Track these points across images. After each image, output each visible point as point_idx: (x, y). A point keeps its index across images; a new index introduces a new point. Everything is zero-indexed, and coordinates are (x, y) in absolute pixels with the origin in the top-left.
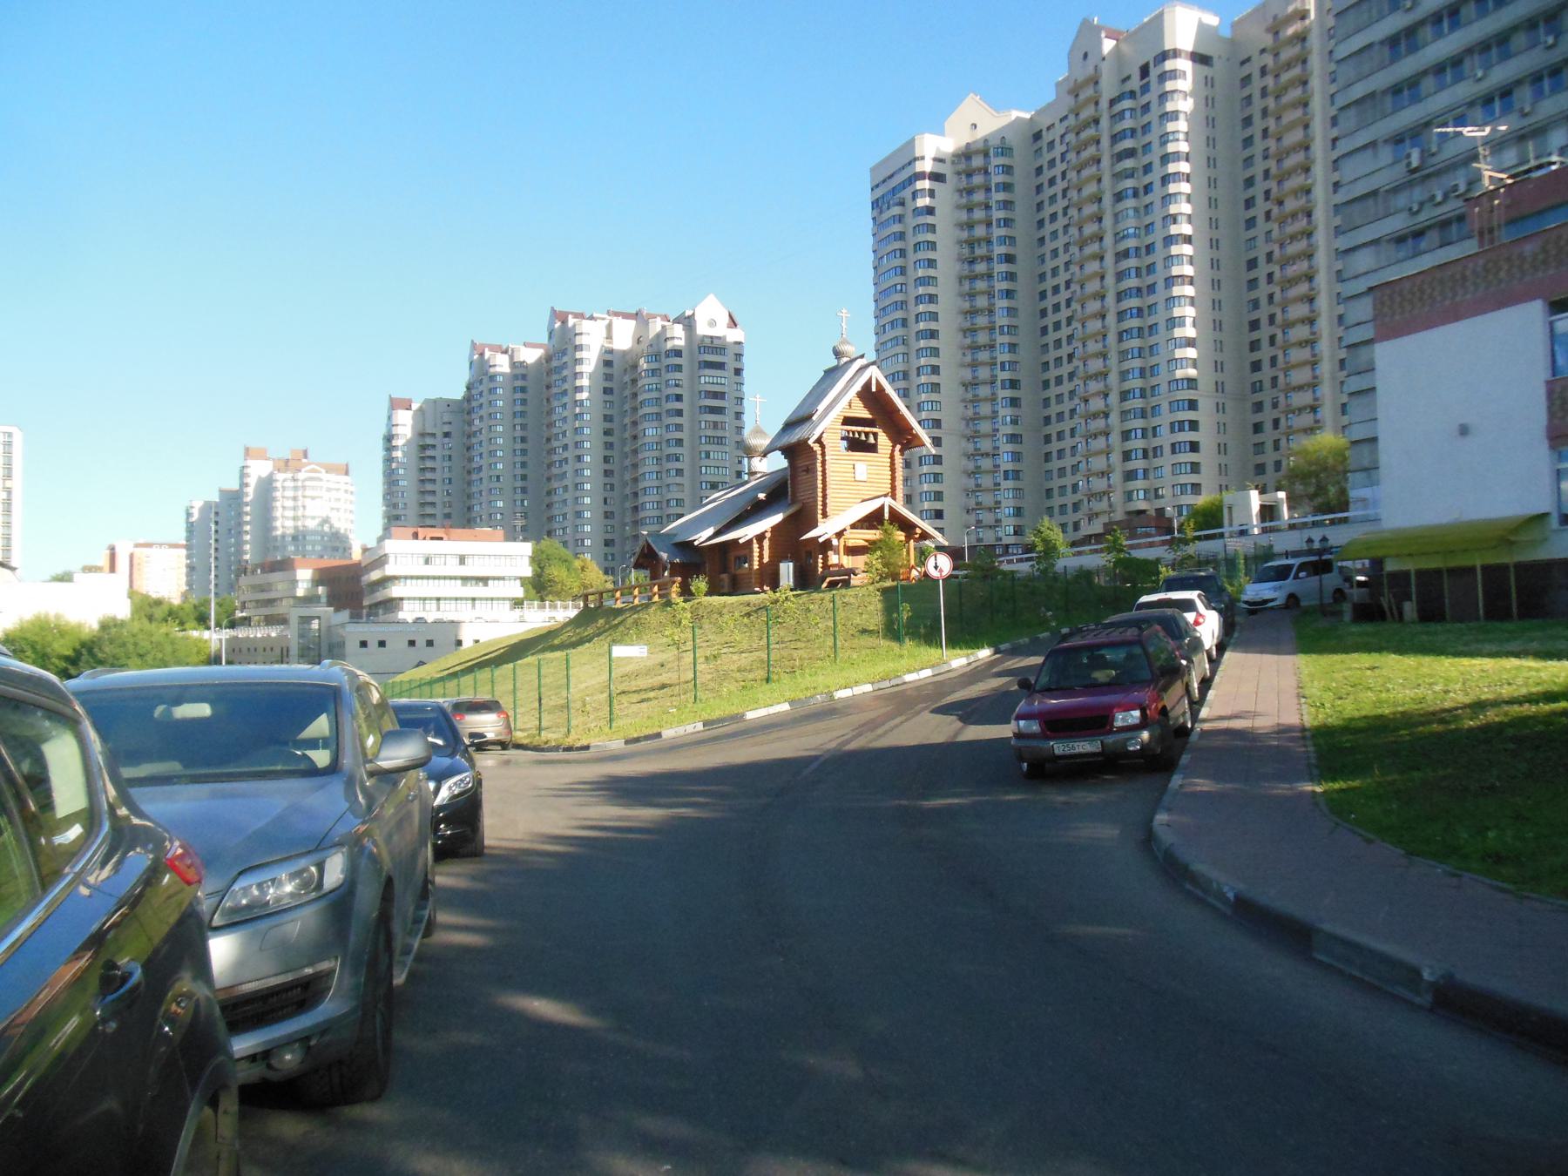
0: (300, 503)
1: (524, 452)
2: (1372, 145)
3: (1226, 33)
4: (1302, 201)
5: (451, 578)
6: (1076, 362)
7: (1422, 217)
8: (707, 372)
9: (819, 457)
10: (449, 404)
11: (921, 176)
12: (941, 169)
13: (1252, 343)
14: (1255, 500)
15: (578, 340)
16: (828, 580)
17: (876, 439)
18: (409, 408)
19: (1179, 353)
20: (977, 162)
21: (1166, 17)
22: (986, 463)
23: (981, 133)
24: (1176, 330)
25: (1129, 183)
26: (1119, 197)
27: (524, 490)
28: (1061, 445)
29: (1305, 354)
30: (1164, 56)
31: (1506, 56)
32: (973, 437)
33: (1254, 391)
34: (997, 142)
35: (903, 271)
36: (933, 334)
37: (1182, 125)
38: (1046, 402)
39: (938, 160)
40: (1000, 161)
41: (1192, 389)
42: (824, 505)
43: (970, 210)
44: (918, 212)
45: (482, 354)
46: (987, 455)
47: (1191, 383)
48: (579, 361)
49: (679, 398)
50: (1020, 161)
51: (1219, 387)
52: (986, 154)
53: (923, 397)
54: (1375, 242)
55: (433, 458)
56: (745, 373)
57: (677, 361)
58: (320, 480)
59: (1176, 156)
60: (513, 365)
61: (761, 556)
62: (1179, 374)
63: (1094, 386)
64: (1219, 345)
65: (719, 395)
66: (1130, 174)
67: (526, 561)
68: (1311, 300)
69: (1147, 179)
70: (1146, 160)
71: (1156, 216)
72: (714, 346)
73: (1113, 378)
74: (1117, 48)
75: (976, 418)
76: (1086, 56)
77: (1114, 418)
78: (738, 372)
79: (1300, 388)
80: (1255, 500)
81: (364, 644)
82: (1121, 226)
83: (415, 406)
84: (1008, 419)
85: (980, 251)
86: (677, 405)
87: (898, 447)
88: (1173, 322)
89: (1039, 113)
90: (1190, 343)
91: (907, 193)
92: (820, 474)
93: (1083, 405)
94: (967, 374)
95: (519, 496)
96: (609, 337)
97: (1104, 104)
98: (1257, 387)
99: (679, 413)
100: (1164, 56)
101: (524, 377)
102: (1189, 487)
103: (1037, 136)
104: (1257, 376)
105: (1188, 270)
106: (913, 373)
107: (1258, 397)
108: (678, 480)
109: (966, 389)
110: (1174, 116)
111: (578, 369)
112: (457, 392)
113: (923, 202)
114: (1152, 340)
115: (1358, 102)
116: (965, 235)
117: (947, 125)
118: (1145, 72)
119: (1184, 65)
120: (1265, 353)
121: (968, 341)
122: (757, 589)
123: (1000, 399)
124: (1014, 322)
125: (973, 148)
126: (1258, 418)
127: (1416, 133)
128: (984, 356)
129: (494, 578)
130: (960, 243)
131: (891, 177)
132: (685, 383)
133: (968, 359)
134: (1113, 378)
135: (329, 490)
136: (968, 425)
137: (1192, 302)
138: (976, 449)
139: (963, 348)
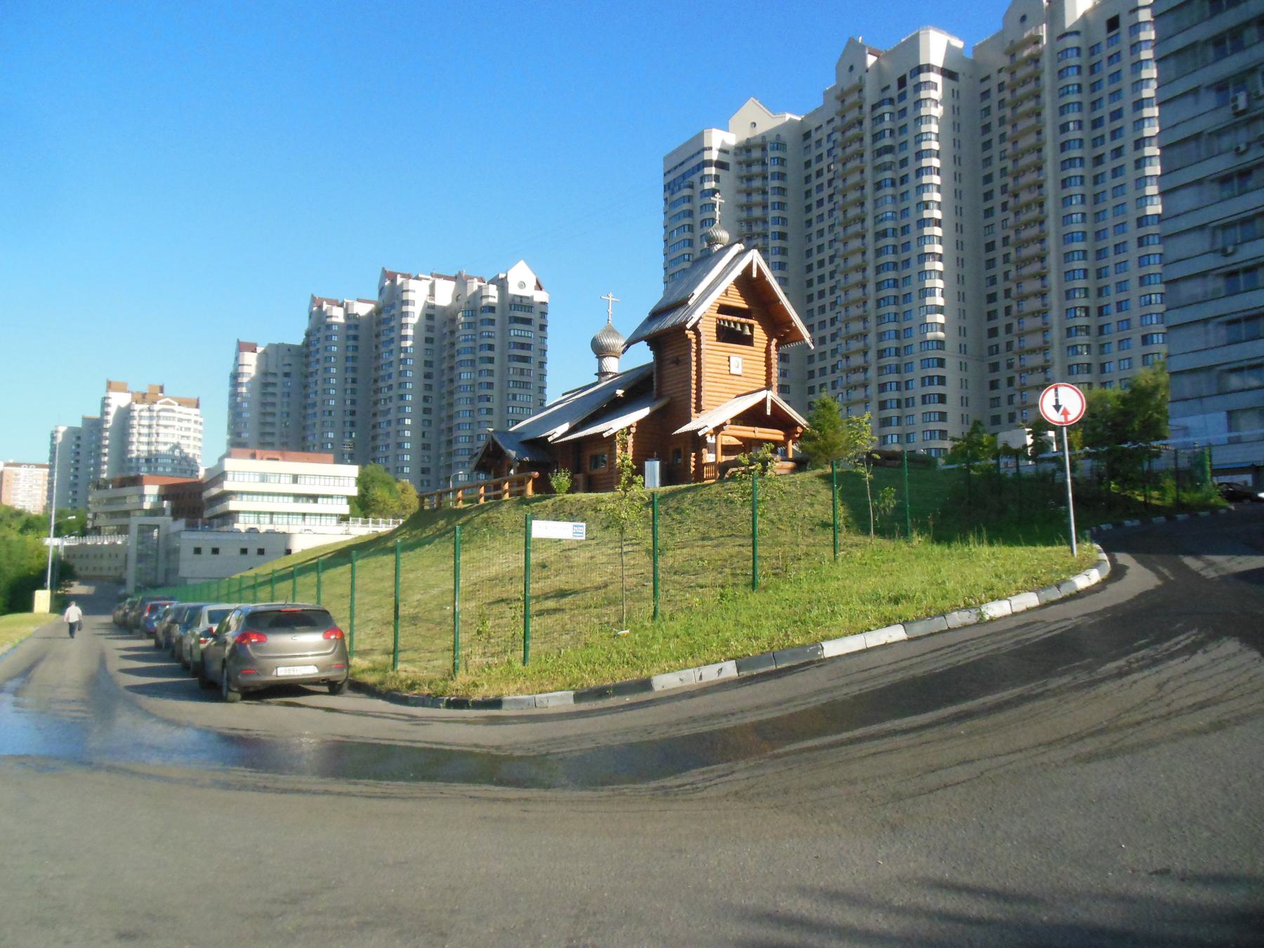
0: (154, 431)
2: (1195, 92)
3: (969, 55)
6: (838, 325)
9: (694, 345)
10: (290, 348)
11: (708, 163)
12: (725, 159)
15: (405, 297)
18: (254, 351)
20: (756, 154)
23: (759, 130)
25: (888, 174)
26: (879, 186)
27: (353, 424)
29: (1038, 322)
30: (920, 69)
33: (991, 354)
35: (691, 228)
42: (699, 398)
45: (320, 307)
47: (940, 343)
48: (406, 314)
49: (491, 347)
51: (963, 349)
52: (764, 149)
54: (1198, 182)
56: (548, 329)
57: (491, 316)
58: (173, 411)
59: (930, 153)
62: (930, 335)
63: (855, 345)
67: (353, 482)
70: (902, 156)
71: (911, 203)
72: (523, 304)
73: (872, 338)
74: (877, 63)
76: (851, 68)
77: (872, 373)
78: (543, 327)
79: (1033, 351)
82: (880, 211)
83: (260, 350)
86: (489, 354)
87: (774, 341)
89: (808, 116)
91: (695, 178)
92: (694, 364)
93: (844, 361)
95: (348, 429)
96: (432, 294)
97: (867, 108)
98: (994, 350)
99: (491, 360)
100: (920, 69)
101: (356, 327)
103: (807, 135)
107: (994, 359)
111: (404, 320)
116: (744, 215)
118: (902, 82)
119: (936, 78)
120: (1001, 322)
125: (753, 142)
130: (740, 221)
131: (682, 163)
132: (498, 335)
134: (872, 338)
135: (180, 420)
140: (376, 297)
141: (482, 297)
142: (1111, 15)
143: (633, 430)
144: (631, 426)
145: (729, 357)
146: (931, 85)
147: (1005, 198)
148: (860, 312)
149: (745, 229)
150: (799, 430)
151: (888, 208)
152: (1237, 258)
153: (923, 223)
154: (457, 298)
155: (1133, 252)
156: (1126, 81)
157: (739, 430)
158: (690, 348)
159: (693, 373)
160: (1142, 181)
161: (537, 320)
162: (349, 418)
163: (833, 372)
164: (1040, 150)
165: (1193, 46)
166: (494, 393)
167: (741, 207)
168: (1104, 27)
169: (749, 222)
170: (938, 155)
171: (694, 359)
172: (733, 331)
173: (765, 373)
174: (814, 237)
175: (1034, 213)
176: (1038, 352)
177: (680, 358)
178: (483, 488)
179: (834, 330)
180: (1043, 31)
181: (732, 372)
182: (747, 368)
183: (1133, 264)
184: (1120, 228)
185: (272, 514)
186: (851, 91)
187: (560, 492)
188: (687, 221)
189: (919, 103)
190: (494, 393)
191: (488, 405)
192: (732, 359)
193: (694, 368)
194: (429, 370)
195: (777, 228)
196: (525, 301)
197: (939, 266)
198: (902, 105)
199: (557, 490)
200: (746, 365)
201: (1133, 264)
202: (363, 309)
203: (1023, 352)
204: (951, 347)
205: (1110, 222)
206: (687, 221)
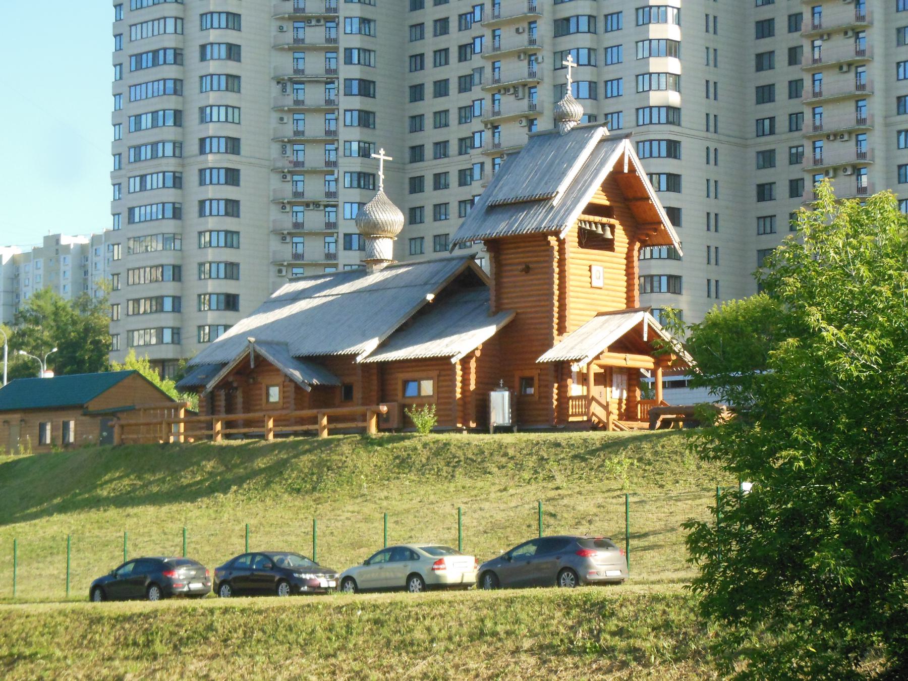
6: (476, 61)
9: (556, 254)
13: (759, 57)
16: (662, 417)
17: (613, 233)
19: (657, 64)
22: (314, 220)
24: (652, 27)
29: (847, 83)
32: (292, 173)
33: (760, 133)
38: (416, 122)
41: (672, 123)
42: (562, 318)
46: (317, 205)
47: (673, 114)
51: (712, 123)
53: (213, 98)
61: (465, 381)
62: (656, 98)
63: (510, 105)
64: (712, 57)
75: (298, 139)
79: (837, 136)
84: (355, 146)
87: (638, 245)
90: (672, 48)
92: (556, 276)
93: (487, 134)
94: (285, 64)
98: (765, 127)
102: (664, 280)
104: (766, 110)
106: (193, 54)
107: (766, 143)
109: (284, 90)
122: (459, 425)
123: (341, 112)
126: (765, 176)
128: (315, 35)
133: (288, 38)
136: (284, 151)
138: (296, 194)
143: (478, 353)
144: (477, 349)
145: (590, 267)
148: (522, 41)
150: (674, 357)
157: (614, 358)
158: (551, 257)
159: (556, 287)
171: (557, 270)
172: (591, 232)
173: (625, 284)
176: (846, 137)
177: (531, 266)
178: (326, 418)
179: (465, 69)
181: (594, 284)
182: (544, 251)
187: (424, 432)
192: (593, 268)
193: (556, 282)
199: (421, 430)
200: (607, 275)
203: (820, 134)
204: (692, 120)
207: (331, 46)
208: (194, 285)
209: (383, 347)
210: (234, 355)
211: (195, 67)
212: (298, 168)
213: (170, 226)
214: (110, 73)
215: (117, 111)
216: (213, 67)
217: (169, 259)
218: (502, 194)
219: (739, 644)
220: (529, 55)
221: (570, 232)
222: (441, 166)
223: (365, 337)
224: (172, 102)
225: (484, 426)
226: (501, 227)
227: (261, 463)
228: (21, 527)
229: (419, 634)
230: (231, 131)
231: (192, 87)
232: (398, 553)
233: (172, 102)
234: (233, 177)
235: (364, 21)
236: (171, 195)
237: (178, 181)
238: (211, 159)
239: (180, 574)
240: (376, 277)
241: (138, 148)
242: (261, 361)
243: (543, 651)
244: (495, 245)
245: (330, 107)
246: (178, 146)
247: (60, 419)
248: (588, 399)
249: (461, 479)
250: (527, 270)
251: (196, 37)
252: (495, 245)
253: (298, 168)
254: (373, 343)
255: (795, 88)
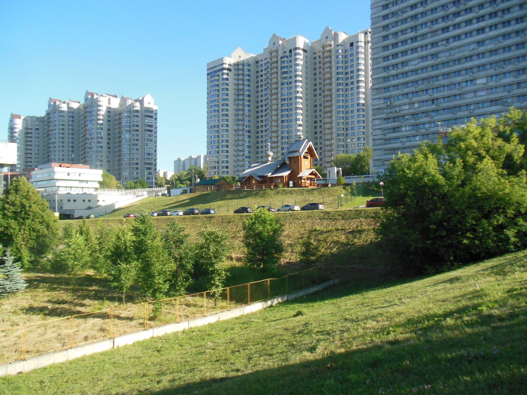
1: (73, 138)
2: (379, 98)
3: (310, 45)
4: (329, 93)
5: (76, 180)
7: (390, 115)
8: (148, 118)
11: (224, 69)
12: (230, 67)
14: (336, 169)
15: (99, 103)
18: (20, 118)
19: (298, 128)
20: (241, 67)
21: (297, 38)
22: (241, 153)
23: (242, 59)
25: (286, 81)
26: (282, 84)
27: (73, 151)
28: (262, 150)
30: (296, 49)
31: (407, 87)
34: (247, 62)
36: (227, 115)
37: (300, 68)
38: (258, 137)
39: (230, 65)
40: (248, 68)
43: (238, 80)
44: (223, 79)
45: (55, 103)
48: (100, 110)
49: (137, 126)
50: (252, 68)
52: (243, 65)
53: (224, 133)
54: (380, 119)
55: (31, 137)
56: (158, 119)
57: (137, 114)
59: (299, 76)
60: (69, 108)
63: (274, 135)
64: (307, 127)
65: (151, 126)
66: (285, 78)
67: (101, 176)
68: (331, 118)
69: (290, 80)
70: (290, 75)
71: (293, 90)
72: (149, 110)
73: (279, 133)
74: (282, 44)
75: (238, 140)
76: (274, 44)
77: (279, 144)
78: (156, 119)
79: (328, 140)
80: (336, 169)
81: (69, 201)
82: (283, 92)
83: (22, 118)
85: (240, 93)
86: (137, 128)
88: (297, 120)
89: (257, 56)
91: (220, 73)
95: (70, 153)
96: (109, 103)
97: (279, 58)
99: (137, 131)
100: (296, 49)
101: (73, 113)
103: (257, 62)
105: (301, 106)
106: (220, 126)
108: (137, 152)
110: (298, 65)
111: (99, 113)
112: (42, 113)
113: (225, 76)
114: (290, 124)
115: (377, 89)
116: (236, 87)
117: (232, 55)
118: (290, 51)
119: (301, 52)
120: (318, 130)
121: (236, 118)
124: (250, 114)
125: (240, 63)
127: (389, 98)
129: (90, 181)
130: (235, 89)
131: (214, 67)
132: (140, 122)
133: (236, 123)
134: (279, 133)
137: (302, 114)
139: (234, 120)
140: (83, 102)
141: (134, 107)
142: (351, 42)
146: (299, 54)
147: (320, 92)
148: (276, 124)
149: (237, 92)
151: (285, 92)
152: (387, 137)
153: (296, 98)
154: (121, 105)
155: (356, 113)
156: (355, 63)
160: (358, 93)
161: (154, 117)
162: (71, 149)
163: (265, 142)
164: (331, 79)
165: (380, 88)
166: (139, 143)
167: (235, 85)
168: (349, 45)
169: (238, 90)
170: (301, 76)
174: (259, 97)
175: (329, 98)
180: (332, 43)
183: (356, 117)
184: (352, 106)
185: (83, 188)
186: (274, 51)
188: (217, 88)
189: (296, 59)
190: (139, 143)
191: (137, 147)
194: (109, 132)
195: (247, 93)
196: (150, 109)
197: (301, 112)
198: (290, 59)
201: (356, 117)
202: (75, 106)
203: (325, 140)
205: (350, 103)
206: (217, 88)
207: (243, 125)
208: (221, 165)
209: (272, 174)
210: (247, 176)
211: (221, 128)
212: (238, 145)
213: (217, 155)
214: (206, 129)
215: (208, 135)
216: (224, 128)
217: (217, 160)
218: (291, 150)
219: (376, 213)
220: (277, 126)
221: (302, 156)
222: (262, 144)
223: (269, 173)
224: (217, 134)
225: (288, 187)
226: (291, 155)
227: (254, 193)
228: (214, 203)
229: (298, 217)
230: (227, 139)
231: (220, 131)
232: (287, 206)
233: (217, 134)
234: (227, 146)
235: (249, 120)
236: (217, 149)
237: (218, 147)
238: (224, 144)
239: (249, 209)
240: (268, 163)
241: (211, 142)
242: (252, 177)
243: (321, 219)
244: (290, 158)
245: (243, 135)
246: (218, 141)
247: (210, 186)
248: (305, 182)
249: (288, 195)
250: (295, 162)
251: (221, 123)
252: (290, 158)
253: (238, 145)
254: (270, 174)
255: (321, 132)
